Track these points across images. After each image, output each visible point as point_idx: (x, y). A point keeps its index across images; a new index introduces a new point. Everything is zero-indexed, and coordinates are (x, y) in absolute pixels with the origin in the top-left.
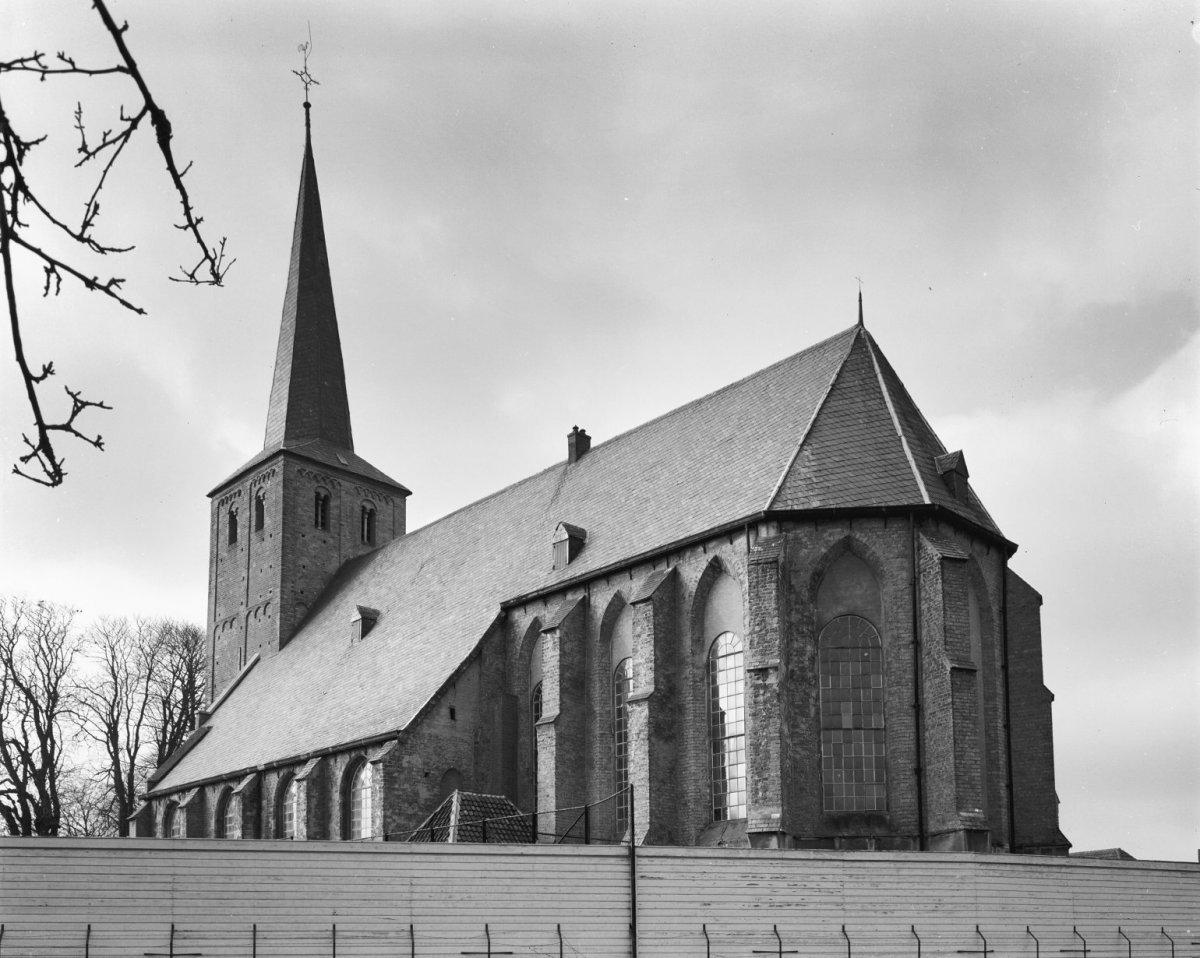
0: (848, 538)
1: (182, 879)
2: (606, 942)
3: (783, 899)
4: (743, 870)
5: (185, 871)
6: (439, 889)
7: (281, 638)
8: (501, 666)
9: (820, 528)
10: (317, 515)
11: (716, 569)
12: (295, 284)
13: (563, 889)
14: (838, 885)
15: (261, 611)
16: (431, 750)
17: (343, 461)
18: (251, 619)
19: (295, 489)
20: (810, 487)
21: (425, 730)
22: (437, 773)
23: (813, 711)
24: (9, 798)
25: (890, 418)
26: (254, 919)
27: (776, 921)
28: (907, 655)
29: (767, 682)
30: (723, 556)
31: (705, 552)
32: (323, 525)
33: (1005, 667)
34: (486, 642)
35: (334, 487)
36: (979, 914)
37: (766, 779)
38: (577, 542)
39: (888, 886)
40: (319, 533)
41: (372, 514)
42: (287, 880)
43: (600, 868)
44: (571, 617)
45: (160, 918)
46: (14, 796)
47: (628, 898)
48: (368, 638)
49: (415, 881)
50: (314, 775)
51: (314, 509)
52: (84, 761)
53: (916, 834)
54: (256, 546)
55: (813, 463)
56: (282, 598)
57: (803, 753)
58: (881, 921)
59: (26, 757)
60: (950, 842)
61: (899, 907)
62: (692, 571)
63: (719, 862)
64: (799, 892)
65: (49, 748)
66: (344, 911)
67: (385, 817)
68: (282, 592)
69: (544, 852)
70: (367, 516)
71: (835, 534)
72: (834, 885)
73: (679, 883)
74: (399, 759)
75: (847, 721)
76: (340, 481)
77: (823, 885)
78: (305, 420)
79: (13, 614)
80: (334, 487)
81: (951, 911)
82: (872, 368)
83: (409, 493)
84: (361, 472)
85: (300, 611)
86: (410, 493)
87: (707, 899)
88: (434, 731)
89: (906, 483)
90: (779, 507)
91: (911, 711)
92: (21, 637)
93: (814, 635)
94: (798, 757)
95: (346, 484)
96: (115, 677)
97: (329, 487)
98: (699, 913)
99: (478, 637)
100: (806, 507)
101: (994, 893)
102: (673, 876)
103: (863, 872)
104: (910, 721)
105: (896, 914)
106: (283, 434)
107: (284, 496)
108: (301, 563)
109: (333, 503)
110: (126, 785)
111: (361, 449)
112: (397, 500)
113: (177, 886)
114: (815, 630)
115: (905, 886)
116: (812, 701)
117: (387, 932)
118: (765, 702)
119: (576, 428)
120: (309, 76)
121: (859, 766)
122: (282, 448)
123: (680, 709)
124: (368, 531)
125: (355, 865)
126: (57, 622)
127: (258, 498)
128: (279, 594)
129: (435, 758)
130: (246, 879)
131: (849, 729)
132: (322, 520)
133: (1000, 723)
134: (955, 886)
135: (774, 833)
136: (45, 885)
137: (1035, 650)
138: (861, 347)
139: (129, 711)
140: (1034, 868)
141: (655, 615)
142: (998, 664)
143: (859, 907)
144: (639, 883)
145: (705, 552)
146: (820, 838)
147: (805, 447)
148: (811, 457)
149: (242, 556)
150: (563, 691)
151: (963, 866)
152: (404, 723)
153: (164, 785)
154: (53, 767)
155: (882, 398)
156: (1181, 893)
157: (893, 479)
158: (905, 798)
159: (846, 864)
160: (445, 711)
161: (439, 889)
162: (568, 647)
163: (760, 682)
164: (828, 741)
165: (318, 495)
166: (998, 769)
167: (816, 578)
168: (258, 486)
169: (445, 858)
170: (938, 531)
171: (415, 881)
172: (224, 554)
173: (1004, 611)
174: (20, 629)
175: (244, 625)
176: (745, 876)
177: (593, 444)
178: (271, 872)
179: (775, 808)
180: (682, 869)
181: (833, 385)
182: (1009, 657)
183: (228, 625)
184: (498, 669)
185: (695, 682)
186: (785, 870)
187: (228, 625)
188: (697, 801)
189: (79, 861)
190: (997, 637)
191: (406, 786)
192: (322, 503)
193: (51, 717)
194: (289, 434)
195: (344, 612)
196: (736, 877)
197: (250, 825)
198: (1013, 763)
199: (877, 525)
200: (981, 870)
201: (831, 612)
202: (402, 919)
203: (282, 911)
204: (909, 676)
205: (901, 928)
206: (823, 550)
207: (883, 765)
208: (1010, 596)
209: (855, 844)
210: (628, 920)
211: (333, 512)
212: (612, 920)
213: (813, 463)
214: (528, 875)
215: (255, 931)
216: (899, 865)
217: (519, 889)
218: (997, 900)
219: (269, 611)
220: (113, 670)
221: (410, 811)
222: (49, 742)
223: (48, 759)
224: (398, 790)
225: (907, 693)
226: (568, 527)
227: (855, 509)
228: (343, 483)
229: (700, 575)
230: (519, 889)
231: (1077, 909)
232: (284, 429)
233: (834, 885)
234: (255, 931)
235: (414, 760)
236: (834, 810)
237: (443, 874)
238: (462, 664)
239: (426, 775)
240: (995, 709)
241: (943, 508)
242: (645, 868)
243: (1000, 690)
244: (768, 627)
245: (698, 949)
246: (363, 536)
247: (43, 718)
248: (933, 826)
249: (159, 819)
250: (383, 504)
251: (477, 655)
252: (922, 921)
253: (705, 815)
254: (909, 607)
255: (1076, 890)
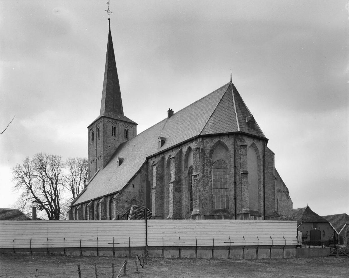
0: (219, 140)
1: (50, 229)
2: (141, 241)
3: (181, 231)
4: (172, 224)
5: (50, 227)
6: (103, 230)
7: (104, 165)
8: (146, 173)
9: (212, 139)
10: (112, 132)
11: (190, 149)
12: (107, 70)
13: (131, 230)
14: (195, 228)
15: (99, 158)
16: (128, 195)
17: (119, 117)
18: (97, 160)
19: (106, 126)
20: (211, 128)
21: (126, 190)
22: (129, 201)
23: (210, 185)
24: (47, 206)
25: (234, 108)
26: (64, 237)
27: (180, 236)
28: (233, 170)
29: (197, 178)
30: (191, 146)
31: (187, 145)
32: (114, 135)
33: (264, 171)
34: (142, 168)
35: (117, 125)
36: (230, 234)
37: (196, 202)
38: (163, 141)
39: (207, 228)
40: (113, 137)
41: (127, 131)
42: (71, 228)
43: (139, 225)
44: (159, 161)
45: (45, 237)
46: (49, 206)
47: (146, 231)
48: (121, 166)
49: (98, 228)
50: (103, 201)
51: (112, 131)
52: (66, 197)
53: (234, 214)
54: (98, 141)
55: (213, 121)
56: (104, 155)
57: (207, 195)
58: (205, 236)
59: (51, 195)
60: (240, 216)
61: (210, 232)
62: (185, 150)
63: (166, 223)
64: (185, 229)
65: (56, 192)
66: (83, 235)
67: (116, 212)
68: (104, 153)
69: (126, 222)
70: (126, 131)
71: (216, 140)
72: (194, 228)
73: (157, 228)
74: (120, 198)
75: (219, 187)
76: (119, 123)
77: (191, 228)
78: (110, 107)
79: (46, 159)
80: (117, 125)
81: (223, 233)
82: (232, 94)
83: (137, 124)
84: (124, 120)
85: (109, 158)
86: (137, 124)
87: (164, 231)
88: (128, 190)
89: (235, 126)
90: (202, 134)
91: (234, 184)
92: (48, 165)
93: (211, 166)
94: (206, 196)
95: (120, 124)
96: (73, 174)
97: (116, 125)
98: (162, 234)
99: (140, 166)
100: (209, 133)
101: (234, 229)
102: (156, 226)
103: (201, 224)
104: (233, 186)
105: (209, 234)
106: (104, 111)
107: (104, 128)
108: (109, 145)
109: (116, 129)
110: (57, 205)
111: (125, 114)
112: (134, 127)
113: (49, 230)
114: (211, 164)
115: (211, 228)
116: (210, 182)
117: (92, 239)
118: (196, 183)
119: (169, 109)
120: (110, 11)
121: (222, 198)
122: (103, 115)
123: (182, 184)
124: (127, 135)
125: (86, 225)
126: (57, 160)
127: (98, 128)
128: (103, 154)
129: (129, 197)
130: (62, 228)
131: (220, 189)
132: (114, 134)
133: (262, 186)
134: (224, 227)
135: (197, 215)
136: (22, 230)
137: (271, 166)
138: (231, 88)
139: (76, 183)
140: (246, 223)
141: (175, 161)
142: (262, 170)
143: (200, 232)
144: (148, 228)
145: (187, 145)
146: (211, 216)
147: (211, 117)
148: (213, 120)
149: (95, 144)
150: (157, 180)
151: (226, 223)
152: (120, 189)
153: (75, 204)
154: (58, 198)
155: (233, 102)
156: (290, 228)
157: (232, 125)
158: (232, 205)
159: (197, 223)
160: (131, 185)
161: (103, 230)
162: (158, 169)
163: (195, 178)
164: (214, 192)
165: (113, 127)
166: (261, 197)
167: (212, 151)
168: (98, 125)
169: (105, 223)
170: (242, 138)
171: (98, 228)
172: (91, 143)
173: (264, 157)
174: (48, 163)
175: (96, 162)
176: (172, 226)
177: (174, 113)
178: (67, 227)
179: (198, 209)
180: (158, 224)
181: (221, 100)
182: (265, 168)
183: (92, 162)
184: (145, 174)
185: (185, 177)
186: (182, 224)
187: (92, 162)
188: (185, 207)
189: (29, 225)
190: (262, 163)
191: (122, 204)
192: (114, 129)
193: (56, 184)
194: (106, 111)
195: (116, 160)
196: (170, 226)
197: (91, 214)
198: (265, 195)
199: (226, 137)
200: (230, 224)
201: (215, 159)
202: (95, 236)
203: (70, 235)
204: (233, 175)
205: (210, 237)
206: (213, 144)
207: (227, 197)
208: (266, 153)
209: (220, 218)
210: (145, 236)
211: (117, 131)
212: (142, 236)
213: (213, 121)
214: (123, 226)
215: (64, 239)
216: (210, 223)
217: (121, 230)
218: (235, 231)
219: (101, 158)
220: (72, 172)
221: (123, 210)
222: (56, 191)
223: (56, 195)
224: (119, 205)
225: (233, 179)
226: (161, 138)
227: (222, 133)
228: (119, 123)
229: (186, 151)
230: (121, 230)
231: (258, 232)
232: (104, 110)
233: (194, 228)
234: (64, 239)
235: (123, 198)
236: (215, 209)
237: (104, 227)
238: (136, 174)
239: (127, 201)
240: (260, 182)
241: (242, 132)
242: (149, 225)
243: (262, 177)
244: (198, 165)
245: (195, 244)
246: (125, 137)
247: (54, 185)
248: (238, 212)
249: (74, 212)
250: (130, 128)
251: (140, 171)
252: (215, 235)
253: (187, 210)
254: (234, 158)
255: (258, 228)
